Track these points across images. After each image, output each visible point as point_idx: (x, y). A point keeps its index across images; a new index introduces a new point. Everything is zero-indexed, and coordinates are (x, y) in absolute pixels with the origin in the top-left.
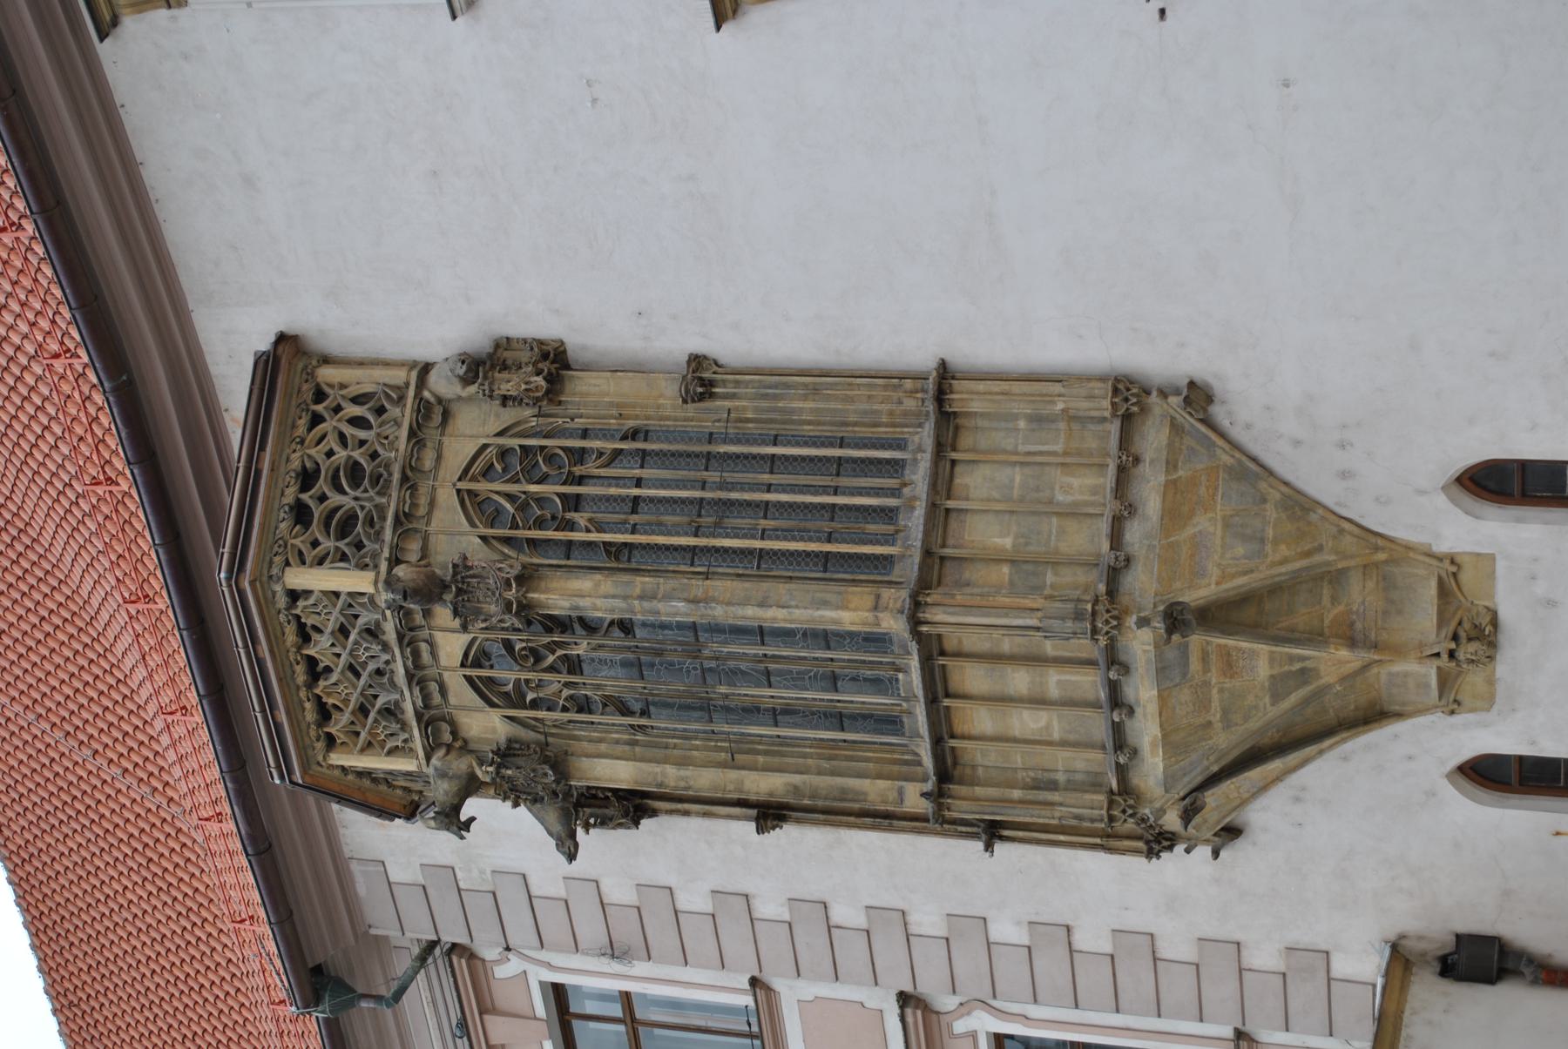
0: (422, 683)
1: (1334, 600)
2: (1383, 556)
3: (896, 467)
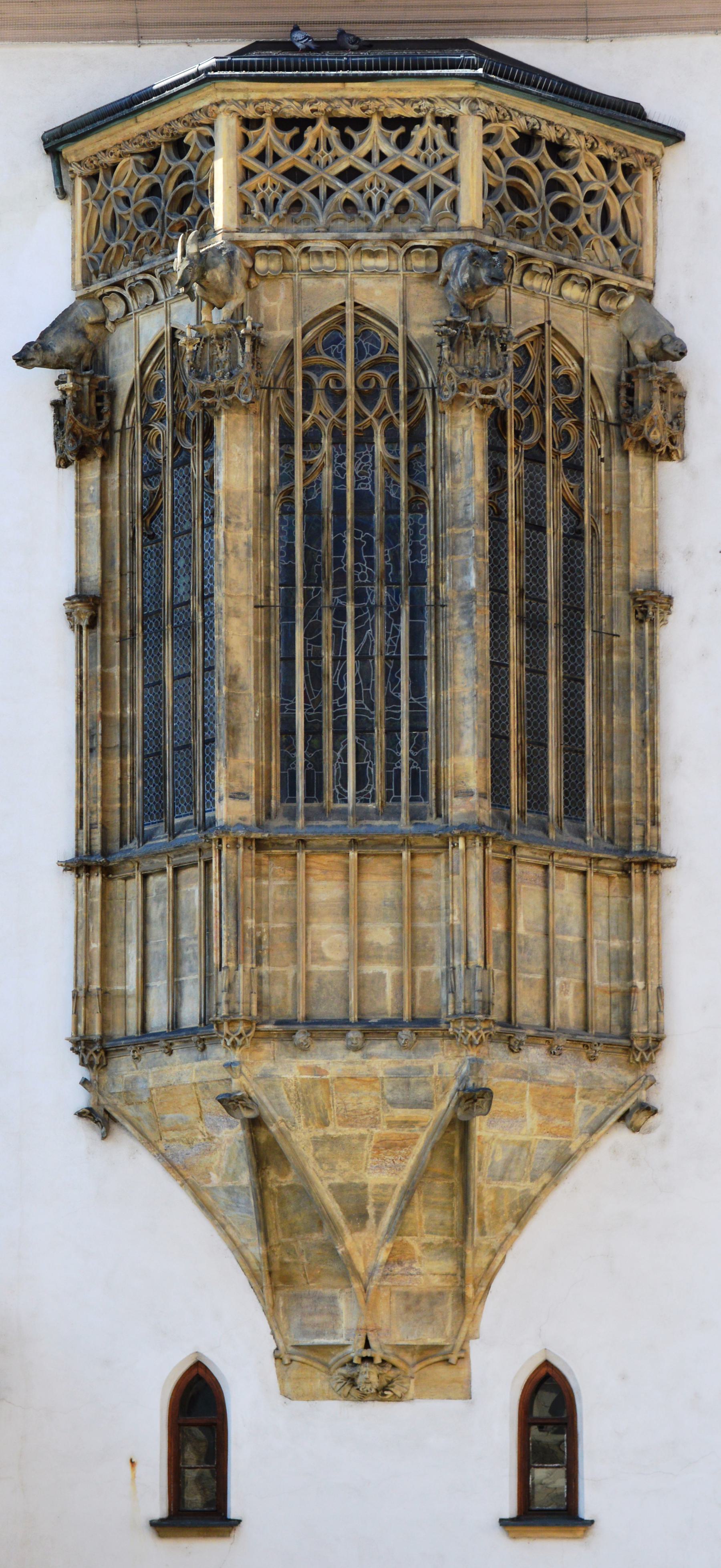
1: (428, 1246)
2: (465, 1294)
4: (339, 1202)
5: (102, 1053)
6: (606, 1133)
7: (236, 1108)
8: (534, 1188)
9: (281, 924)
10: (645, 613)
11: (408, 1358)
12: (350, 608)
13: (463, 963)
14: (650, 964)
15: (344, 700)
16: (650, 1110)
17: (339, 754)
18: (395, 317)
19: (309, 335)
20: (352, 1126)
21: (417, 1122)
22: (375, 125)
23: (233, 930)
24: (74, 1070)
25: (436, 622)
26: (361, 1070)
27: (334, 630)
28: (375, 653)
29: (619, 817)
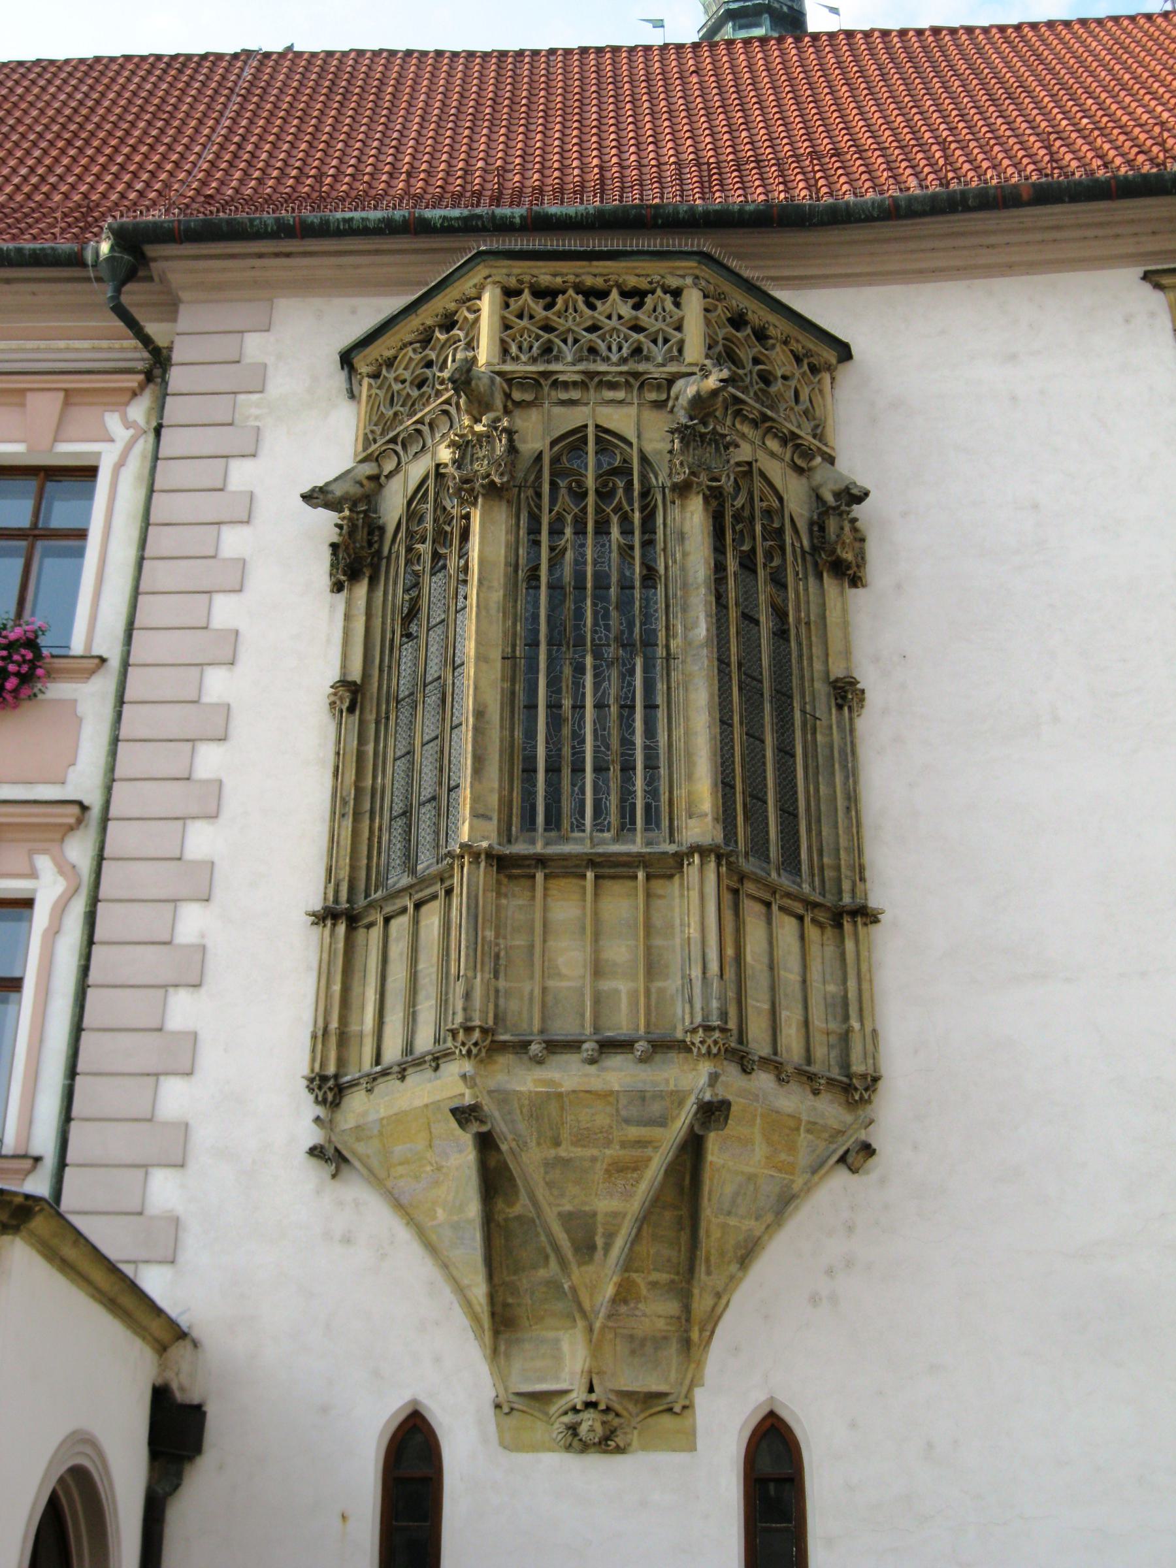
0: (582, 385)
1: (654, 1285)
2: (690, 1336)
3: (553, 821)
4: (568, 1232)
5: (336, 1089)
6: (827, 1173)
7: (468, 1121)
8: (758, 1228)
9: (519, 941)
10: (844, 698)
11: (631, 1406)
12: (589, 660)
13: (700, 975)
14: (865, 1006)
15: (583, 741)
16: (868, 1150)
17: (576, 789)
18: (632, 437)
19: (556, 448)
20: (584, 1146)
21: (650, 1142)
22: (615, 294)
23: (472, 939)
24: (308, 1108)
25: (668, 675)
26: (596, 1084)
27: (573, 683)
28: (611, 701)
29: (829, 874)
